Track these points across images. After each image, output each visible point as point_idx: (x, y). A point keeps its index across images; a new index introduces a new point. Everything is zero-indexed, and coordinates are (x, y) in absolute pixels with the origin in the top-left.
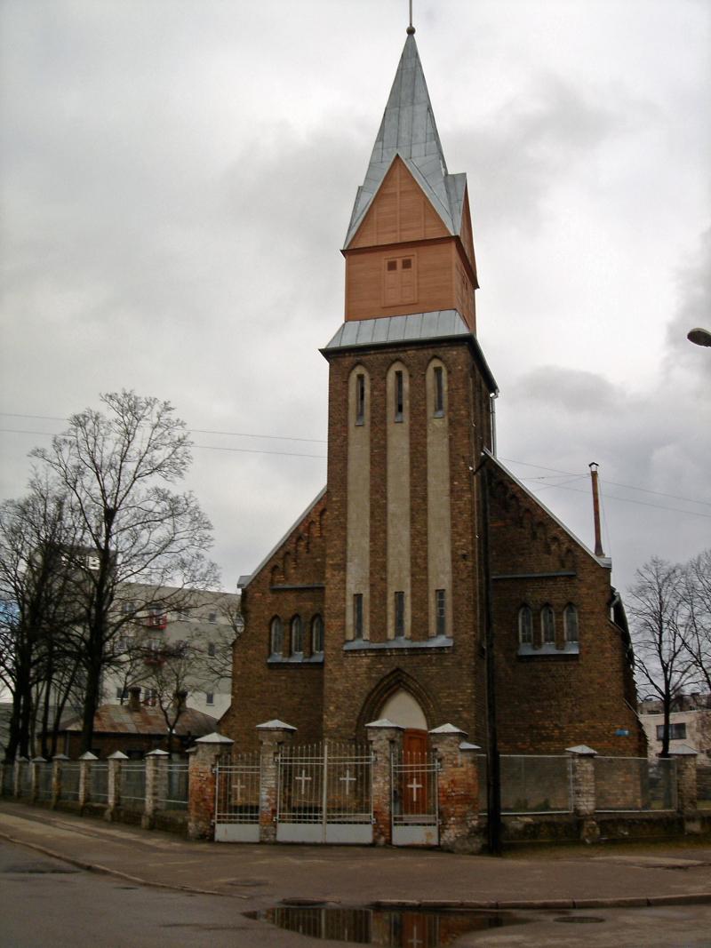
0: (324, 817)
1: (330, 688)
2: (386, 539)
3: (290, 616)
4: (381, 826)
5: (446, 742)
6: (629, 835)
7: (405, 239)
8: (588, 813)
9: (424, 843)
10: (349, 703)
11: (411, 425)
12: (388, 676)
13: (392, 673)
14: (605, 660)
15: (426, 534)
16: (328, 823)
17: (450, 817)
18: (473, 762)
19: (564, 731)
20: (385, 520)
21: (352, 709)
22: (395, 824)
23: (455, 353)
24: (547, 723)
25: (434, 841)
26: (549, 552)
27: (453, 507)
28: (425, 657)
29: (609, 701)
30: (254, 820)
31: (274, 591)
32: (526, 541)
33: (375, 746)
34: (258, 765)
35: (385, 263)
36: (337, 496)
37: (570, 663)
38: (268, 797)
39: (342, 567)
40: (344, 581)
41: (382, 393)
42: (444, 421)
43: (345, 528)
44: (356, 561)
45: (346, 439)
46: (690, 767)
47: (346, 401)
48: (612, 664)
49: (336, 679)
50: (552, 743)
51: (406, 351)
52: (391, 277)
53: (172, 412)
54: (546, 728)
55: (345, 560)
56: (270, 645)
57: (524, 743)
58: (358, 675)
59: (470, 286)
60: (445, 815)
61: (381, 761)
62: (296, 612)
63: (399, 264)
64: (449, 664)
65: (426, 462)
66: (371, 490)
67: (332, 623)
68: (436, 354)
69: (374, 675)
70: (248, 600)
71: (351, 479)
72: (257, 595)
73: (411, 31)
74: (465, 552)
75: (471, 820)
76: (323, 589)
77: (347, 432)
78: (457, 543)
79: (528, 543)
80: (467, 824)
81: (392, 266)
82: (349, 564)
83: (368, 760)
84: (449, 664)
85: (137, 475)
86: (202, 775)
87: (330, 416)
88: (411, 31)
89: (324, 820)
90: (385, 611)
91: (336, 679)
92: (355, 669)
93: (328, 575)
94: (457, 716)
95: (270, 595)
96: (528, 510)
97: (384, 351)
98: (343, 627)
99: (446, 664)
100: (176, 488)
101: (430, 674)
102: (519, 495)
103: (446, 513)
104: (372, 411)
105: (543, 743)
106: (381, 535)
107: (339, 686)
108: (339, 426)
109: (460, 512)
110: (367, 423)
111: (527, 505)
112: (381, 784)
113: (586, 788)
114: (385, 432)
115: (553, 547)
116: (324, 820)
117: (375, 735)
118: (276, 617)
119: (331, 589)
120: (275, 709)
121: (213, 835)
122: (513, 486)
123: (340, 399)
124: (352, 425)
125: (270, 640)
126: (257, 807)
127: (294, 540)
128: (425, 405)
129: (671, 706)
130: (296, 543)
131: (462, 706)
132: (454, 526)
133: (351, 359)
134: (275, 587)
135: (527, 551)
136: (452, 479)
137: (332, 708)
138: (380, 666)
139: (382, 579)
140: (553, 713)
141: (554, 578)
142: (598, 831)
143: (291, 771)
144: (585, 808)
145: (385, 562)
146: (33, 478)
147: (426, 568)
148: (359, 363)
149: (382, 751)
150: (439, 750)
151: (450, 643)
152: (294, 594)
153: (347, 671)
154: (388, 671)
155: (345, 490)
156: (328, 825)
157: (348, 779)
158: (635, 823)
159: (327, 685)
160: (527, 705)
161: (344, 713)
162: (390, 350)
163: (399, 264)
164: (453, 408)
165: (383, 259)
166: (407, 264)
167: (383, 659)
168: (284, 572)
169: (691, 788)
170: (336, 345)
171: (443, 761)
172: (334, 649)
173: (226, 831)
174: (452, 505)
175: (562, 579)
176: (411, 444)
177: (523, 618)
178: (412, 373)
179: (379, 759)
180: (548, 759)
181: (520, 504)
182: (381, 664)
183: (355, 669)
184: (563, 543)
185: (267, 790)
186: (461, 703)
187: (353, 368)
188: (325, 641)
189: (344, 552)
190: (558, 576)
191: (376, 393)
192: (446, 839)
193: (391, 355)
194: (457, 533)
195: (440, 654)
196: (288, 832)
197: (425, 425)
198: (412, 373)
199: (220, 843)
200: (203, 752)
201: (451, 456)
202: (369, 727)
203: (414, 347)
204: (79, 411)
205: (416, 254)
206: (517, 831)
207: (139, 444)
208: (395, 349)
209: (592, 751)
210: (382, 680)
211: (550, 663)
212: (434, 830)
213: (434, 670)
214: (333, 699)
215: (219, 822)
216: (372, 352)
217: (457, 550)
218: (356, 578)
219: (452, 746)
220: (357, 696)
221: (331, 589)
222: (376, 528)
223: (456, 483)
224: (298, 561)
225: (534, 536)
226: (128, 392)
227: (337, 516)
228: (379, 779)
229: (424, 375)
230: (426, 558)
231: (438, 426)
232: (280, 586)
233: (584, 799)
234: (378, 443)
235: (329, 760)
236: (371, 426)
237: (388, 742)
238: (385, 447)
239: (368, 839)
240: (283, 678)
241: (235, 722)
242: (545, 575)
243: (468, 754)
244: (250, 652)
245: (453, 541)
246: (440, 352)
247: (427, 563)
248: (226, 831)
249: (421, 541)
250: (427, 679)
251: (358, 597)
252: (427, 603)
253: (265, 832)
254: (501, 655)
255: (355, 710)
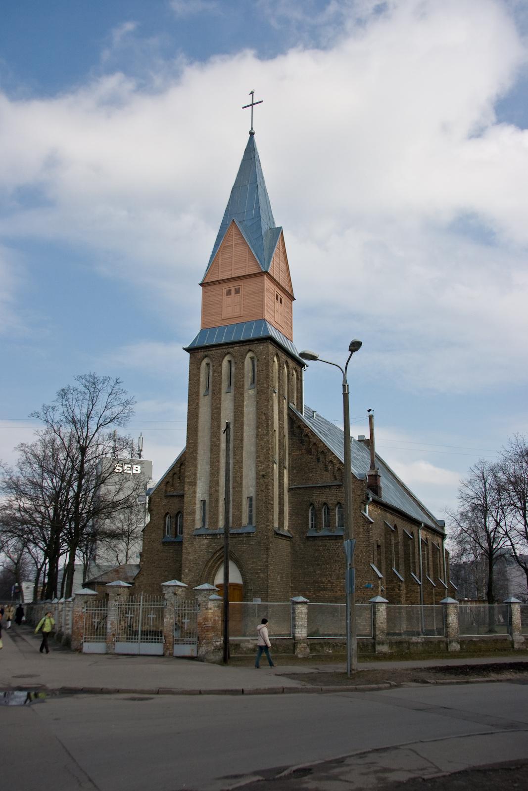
0: (139, 639)
1: (186, 558)
2: (219, 465)
3: (176, 513)
4: (168, 645)
5: (202, 594)
6: (333, 653)
7: (237, 275)
8: (302, 639)
9: (190, 655)
10: (196, 567)
11: (235, 394)
12: (218, 551)
13: (221, 549)
14: (360, 540)
15: (242, 462)
16: (141, 642)
17: (203, 640)
18: (218, 606)
19: (334, 584)
20: (219, 454)
21: (198, 571)
22: (175, 644)
23: (261, 347)
24: (324, 580)
25: (194, 654)
26: (327, 470)
27: (257, 445)
28: (240, 539)
29: (361, 565)
30: (157, 641)
31: (167, 497)
32: (314, 464)
33: (166, 597)
34: (107, 607)
35: (225, 291)
36: (192, 440)
37: (338, 541)
38: (111, 626)
39: (194, 484)
40: (195, 492)
41: (219, 374)
42: (255, 391)
43: (196, 459)
44: (202, 479)
45: (197, 404)
46: (381, 610)
47: (199, 380)
48: (363, 542)
49: (189, 553)
50: (327, 592)
51: (233, 347)
52: (227, 300)
53: (121, 384)
54: (323, 583)
55: (195, 479)
56: (164, 531)
57: (310, 592)
58: (202, 550)
59: (285, 299)
60: (200, 638)
61: (169, 605)
62: (179, 510)
63: (233, 292)
64: (253, 543)
65: (243, 417)
66: (211, 435)
67: (187, 518)
68: (250, 348)
69: (210, 550)
70: (152, 503)
71: (200, 428)
72: (157, 500)
73: (252, 134)
74: (264, 473)
75: (215, 642)
76: (182, 496)
77: (198, 399)
78: (259, 468)
79: (315, 465)
80: (213, 644)
81: (229, 293)
82: (198, 482)
83: (163, 605)
84: (253, 543)
85: (98, 426)
86: (77, 613)
87: (189, 390)
88: (252, 134)
89: (139, 641)
90: (217, 510)
91: (189, 553)
92: (200, 547)
93: (186, 489)
94: (257, 575)
95: (165, 500)
96: (315, 444)
97: (221, 348)
98: (194, 521)
99: (251, 543)
100: (121, 433)
101: (242, 550)
102: (310, 434)
103: (253, 449)
104: (213, 386)
105: (321, 592)
106: (217, 463)
107: (191, 557)
108: (194, 396)
109: (262, 448)
110: (210, 393)
111: (314, 441)
112: (168, 619)
113: (300, 623)
114: (220, 399)
115: (330, 467)
116: (139, 641)
117: (166, 590)
118: (167, 513)
119: (187, 497)
120: (166, 571)
121: (81, 649)
122: (306, 428)
123: (195, 379)
124: (223, 391)
125: (165, 527)
126: (161, 632)
127: (179, 465)
128: (243, 381)
129: (494, 562)
130: (180, 467)
131: (260, 569)
132: (258, 457)
133: (202, 353)
134: (168, 494)
135: (314, 470)
136: (258, 428)
137: (186, 571)
138: (214, 545)
139: (216, 491)
140: (328, 573)
141: (330, 487)
142: (308, 650)
143: (148, 611)
144: (300, 635)
145: (218, 480)
146: (129, 399)
147: (241, 483)
148: (206, 356)
149: (170, 599)
150: (199, 599)
151: (254, 530)
152: (178, 499)
153: (195, 548)
154: (219, 548)
155: (197, 435)
156: (141, 643)
157: (152, 616)
158: (337, 645)
159: (184, 556)
160: (312, 568)
161: (193, 574)
162: (224, 347)
163: (233, 292)
164: (259, 382)
165: (224, 288)
166: (237, 291)
167: (216, 540)
168: (173, 486)
169: (382, 623)
170: (193, 346)
171: (201, 606)
172: (188, 534)
173: (89, 646)
174: (257, 444)
175: (334, 487)
176: (235, 406)
177: (312, 512)
178: (242, 359)
179: (168, 604)
180: (275, 605)
181: (311, 440)
182: (215, 543)
183: (200, 547)
184: (336, 464)
185: (110, 622)
186: (260, 567)
187: (203, 359)
188: (184, 530)
189: (195, 474)
190: (332, 486)
191: (215, 375)
192: (200, 653)
193: (225, 350)
194: (260, 461)
195: (248, 537)
196: (123, 647)
197: (243, 394)
198: (242, 359)
199: (85, 654)
200: (78, 600)
201: (257, 413)
202: (164, 585)
203: (238, 345)
204: (65, 386)
205: (243, 284)
206: (249, 649)
207: (99, 407)
208: (227, 347)
209: (305, 600)
210: (215, 553)
211: (326, 541)
212: (194, 647)
213: (245, 547)
214: (187, 565)
215: (85, 641)
216: (214, 349)
217: (260, 472)
218: (201, 491)
219: (205, 597)
220: (201, 563)
221: (187, 497)
222: (213, 459)
223: (260, 430)
224: (181, 478)
225: (318, 460)
226: (92, 374)
227: (192, 452)
228: (168, 616)
229: (243, 362)
230: (241, 477)
231: (251, 394)
232: (171, 494)
233: (300, 630)
234: (216, 406)
235: (143, 605)
236: (213, 395)
237: (173, 594)
238: (219, 409)
239: (161, 652)
240: (171, 551)
241: (144, 579)
242: (326, 485)
243: (215, 601)
244: (153, 535)
245: (257, 466)
246: (253, 347)
247: (242, 480)
248: (89, 646)
249: (239, 467)
250: (240, 553)
251: (204, 502)
252: (241, 505)
253: (108, 647)
254: (297, 536)
255: (200, 571)
